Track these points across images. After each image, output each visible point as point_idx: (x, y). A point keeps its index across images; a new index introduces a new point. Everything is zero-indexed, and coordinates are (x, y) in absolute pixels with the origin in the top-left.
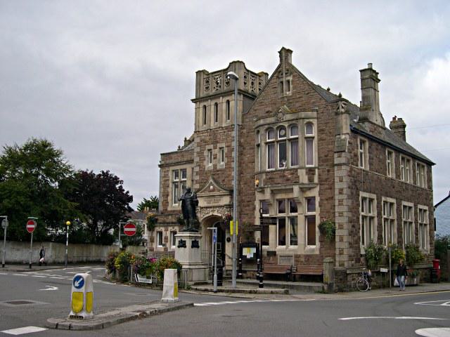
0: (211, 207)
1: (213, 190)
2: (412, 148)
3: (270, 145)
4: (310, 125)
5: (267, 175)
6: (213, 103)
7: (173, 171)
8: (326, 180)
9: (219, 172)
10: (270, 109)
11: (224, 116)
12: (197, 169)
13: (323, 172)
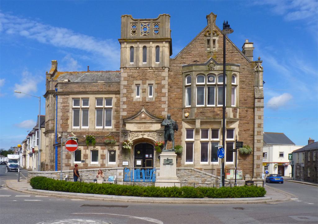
0: (141, 132)
1: (145, 118)
2: (108, 195)
3: (200, 88)
4: (233, 77)
5: (197, 109)
6: (141, 46)
7: (73, 98)
9: (149, 104)
11: (154, 58)
12: (125, 99)
13: (242, 111)
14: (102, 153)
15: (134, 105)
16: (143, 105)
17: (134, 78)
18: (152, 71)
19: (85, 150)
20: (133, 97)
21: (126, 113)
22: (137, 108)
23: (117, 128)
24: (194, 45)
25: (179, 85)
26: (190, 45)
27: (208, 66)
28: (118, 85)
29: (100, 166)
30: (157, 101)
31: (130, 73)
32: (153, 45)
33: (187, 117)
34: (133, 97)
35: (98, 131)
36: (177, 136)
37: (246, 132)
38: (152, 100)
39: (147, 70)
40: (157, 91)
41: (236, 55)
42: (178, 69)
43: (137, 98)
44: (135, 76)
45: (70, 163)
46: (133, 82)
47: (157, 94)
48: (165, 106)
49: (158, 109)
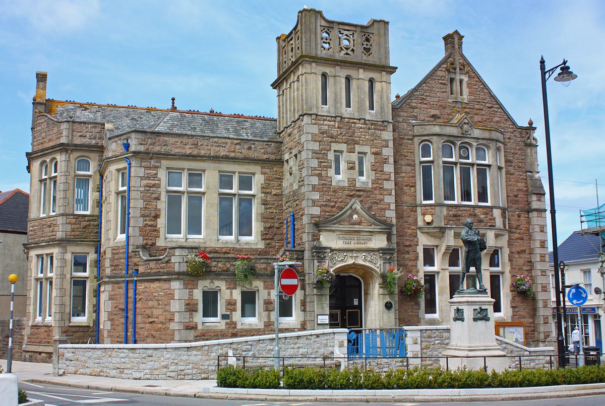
5: (448, 210)
6: (343, 73)
8: (517, 227)
9: (361, 193)
10: (437, 112)
12: (315, 181)
14: (228, 297)
15: (334, 194)
16: (352, 194)
17: (332, 138)
18: (365, 126)
19: (229, 291)
20: (331, 178)
21: (318, 209)
22: (340, 200)
23: (267, 239)
24: (430, 86)
25: (408, 160)
26: (424, 85)
27: (461, 128)
28: (266, 147)
29: (262, 326)
30: (376, 189)
31: (324, 127)
32: (363, 74)
33: (428, 223)
34: (331, 178)
35: (226, 246)
36: (410, 260)
37: (521, 255)
38: (367, 185)
39: (354, 123)
40: (374, 169)
41: (497, 112)
42: (405, 127)
43: (340, 179)
44: (335, 134)
45: (195, 320)
46: (330, 146)
47: (376, 173)
48: (390, 199)
49: (379, 206)
